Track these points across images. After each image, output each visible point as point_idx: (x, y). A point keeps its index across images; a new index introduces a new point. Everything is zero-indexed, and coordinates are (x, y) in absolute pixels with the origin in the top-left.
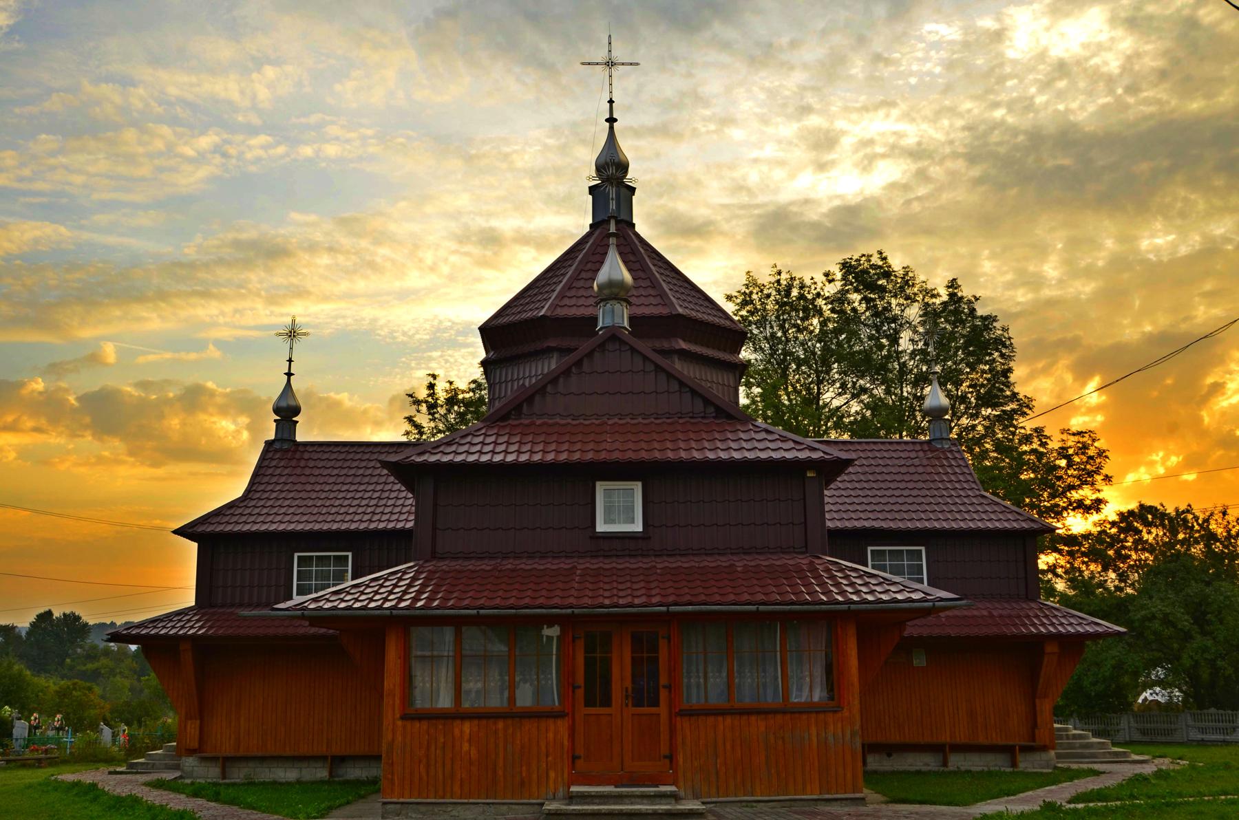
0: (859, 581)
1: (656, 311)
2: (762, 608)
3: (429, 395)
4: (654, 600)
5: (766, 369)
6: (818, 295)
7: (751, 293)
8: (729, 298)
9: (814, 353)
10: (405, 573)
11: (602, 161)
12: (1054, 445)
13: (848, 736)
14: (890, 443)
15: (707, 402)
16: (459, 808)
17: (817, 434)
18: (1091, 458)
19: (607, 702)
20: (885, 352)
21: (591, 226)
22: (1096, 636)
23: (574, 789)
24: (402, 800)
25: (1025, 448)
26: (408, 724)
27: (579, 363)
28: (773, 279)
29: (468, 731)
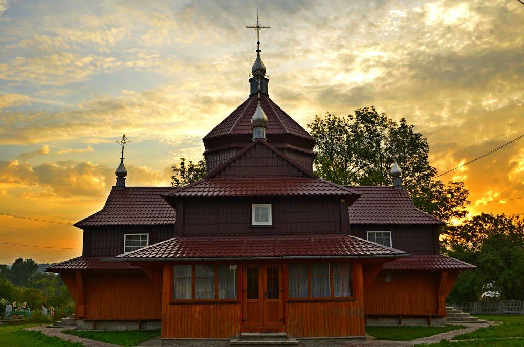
0: (363, 246)
2: (322, 257)
3: (181, 167)
4: (277, 254)
5: (324, 156)
6: (346, 125)
7: (318, 124)
8: (308, 126)
10: (171, 242)
12: (446, 188)
16: (194, 342)
18: (461, 194)
19: (257, 297)
20: (374, 149)
22: (463, 269)
23: (242, 334)
24: (170, 339)
28: (327, 118)
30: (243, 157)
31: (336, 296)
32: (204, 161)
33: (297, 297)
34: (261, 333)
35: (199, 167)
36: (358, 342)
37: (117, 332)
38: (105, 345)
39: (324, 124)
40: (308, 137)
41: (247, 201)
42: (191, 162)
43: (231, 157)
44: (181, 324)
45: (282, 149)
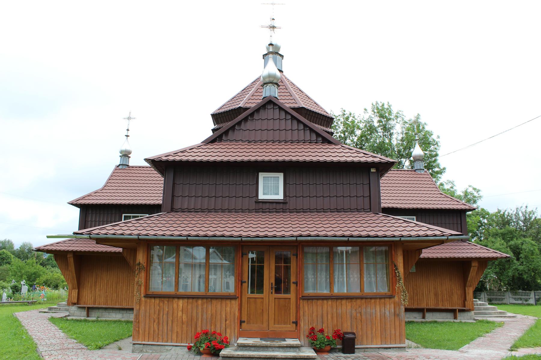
24: (143, 342)
26: (148, 300)
29: (181, 305)
30: (249, 118)
44: (159, 323)
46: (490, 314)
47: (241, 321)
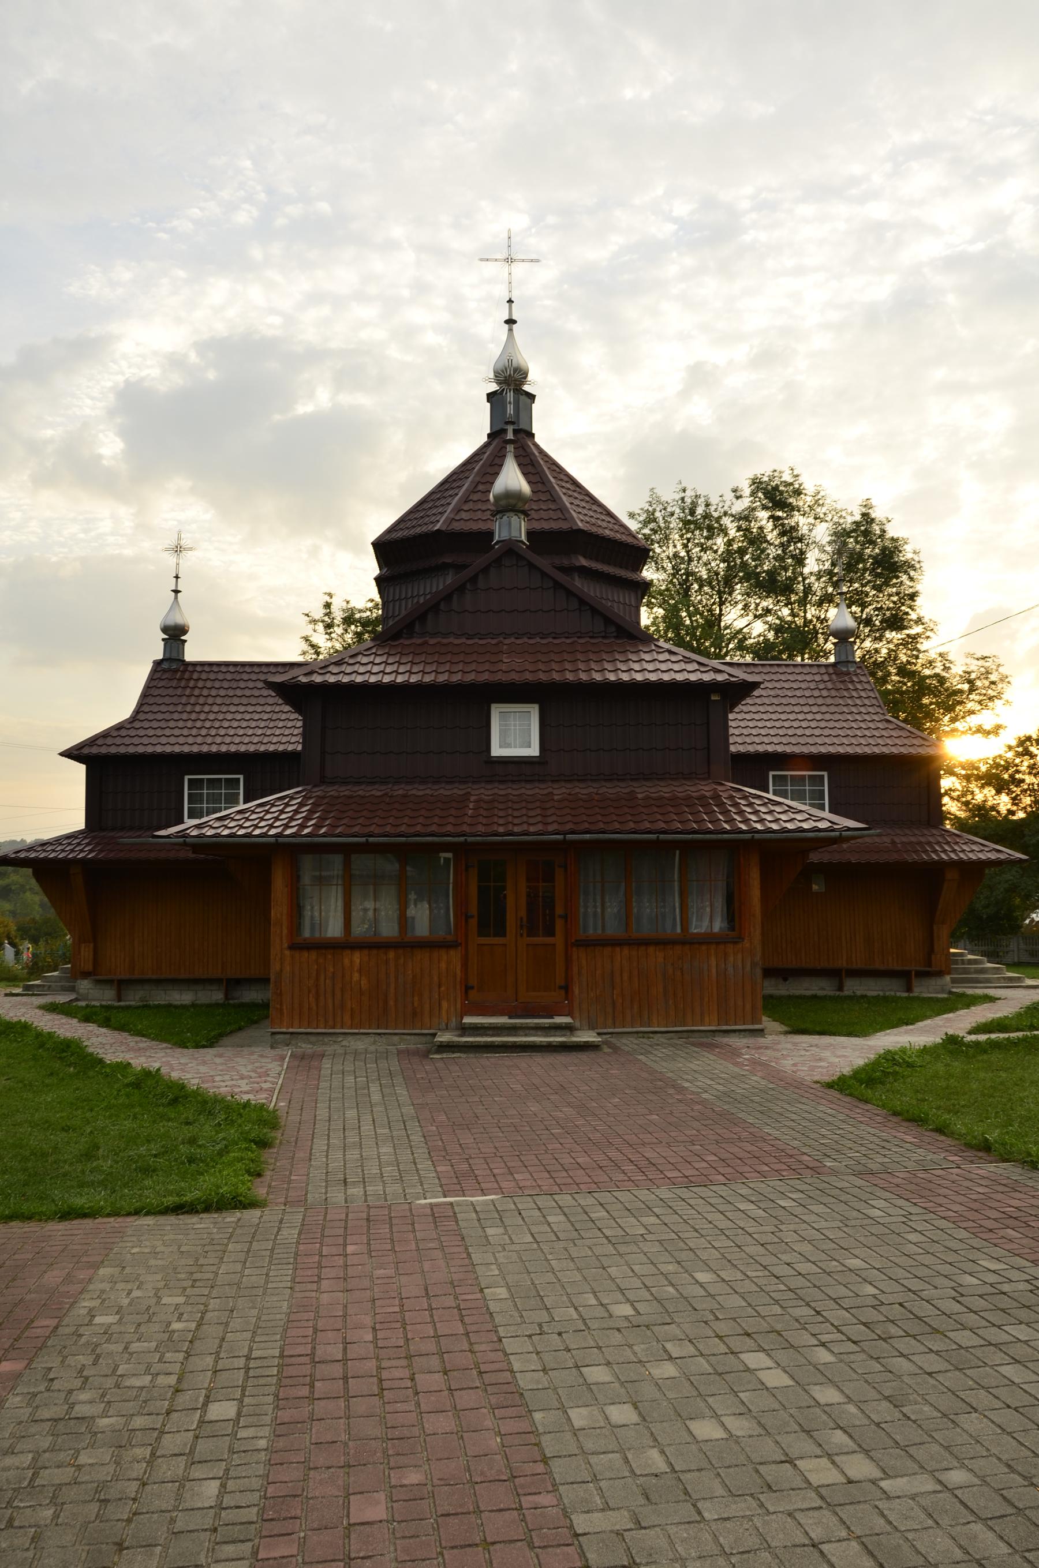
0: (763, 809)
1: (554, 526)
2: (662, 836)
3: (326, 615)
4: (551, 828)
5: (667, 590)
6: (725, 514)
7: (654, 510)
8: (632, 515)
9: (717, 574)
10: (292, 798)
11: (500, 366)
12: (957, 669)
13: (748, 968)
14: (794, 666)
15: (608, 621)
16: (350, 1038)
17: (718, 656)
18: (993, 683)
19: (501, 932)
20: (789, 574)
21: (489, 436)
22: (998, 863)
23: (467, 1020)
24: (291, 1030)
25: (927, 672)
27: (474, 579)
28: (678, 497)
29: (358, 961)
31: (694, 930)
32: (378, 599)
33: (599, 932)
34: (510, 1018)
35: (368, 613)
36: (745, 1041)
37: (169, 1008)
38: (136, 1042)
39: (669, 510)
40: (630, 540)
41: (477, 700)
42: (348, 602)
43: (441, 587)
45: (568, 570)
46: (988, 981)
47: (466, 986)
